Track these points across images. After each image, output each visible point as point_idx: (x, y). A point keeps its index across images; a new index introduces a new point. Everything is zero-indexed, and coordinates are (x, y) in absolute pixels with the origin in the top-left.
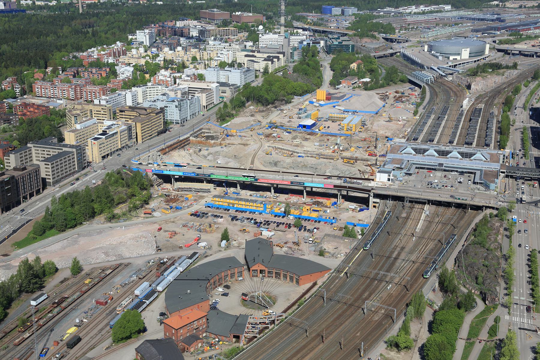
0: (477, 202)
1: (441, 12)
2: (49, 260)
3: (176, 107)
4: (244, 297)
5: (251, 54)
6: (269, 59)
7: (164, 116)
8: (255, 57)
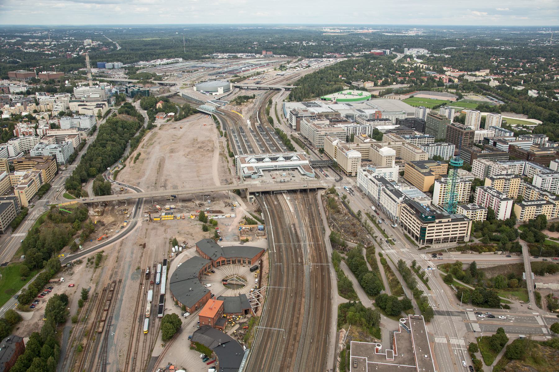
0: (315, 186)
1: (177, 63)
2: (77, 302)
3: (60, 151)
4: (225, 282)
5: (83, 103)
6: (98, 106)
7: (56, 161)
8: (86, 105)
